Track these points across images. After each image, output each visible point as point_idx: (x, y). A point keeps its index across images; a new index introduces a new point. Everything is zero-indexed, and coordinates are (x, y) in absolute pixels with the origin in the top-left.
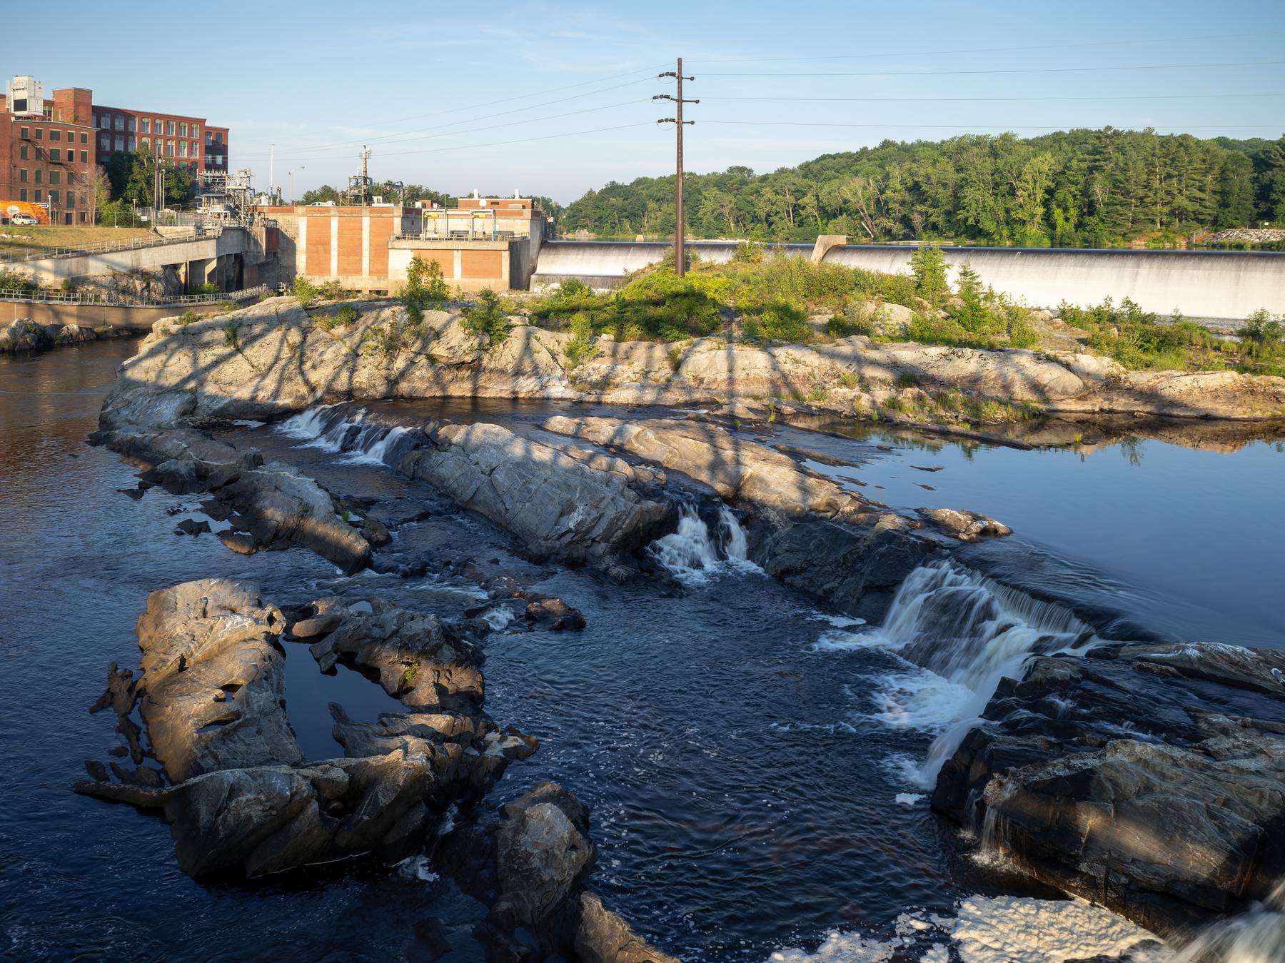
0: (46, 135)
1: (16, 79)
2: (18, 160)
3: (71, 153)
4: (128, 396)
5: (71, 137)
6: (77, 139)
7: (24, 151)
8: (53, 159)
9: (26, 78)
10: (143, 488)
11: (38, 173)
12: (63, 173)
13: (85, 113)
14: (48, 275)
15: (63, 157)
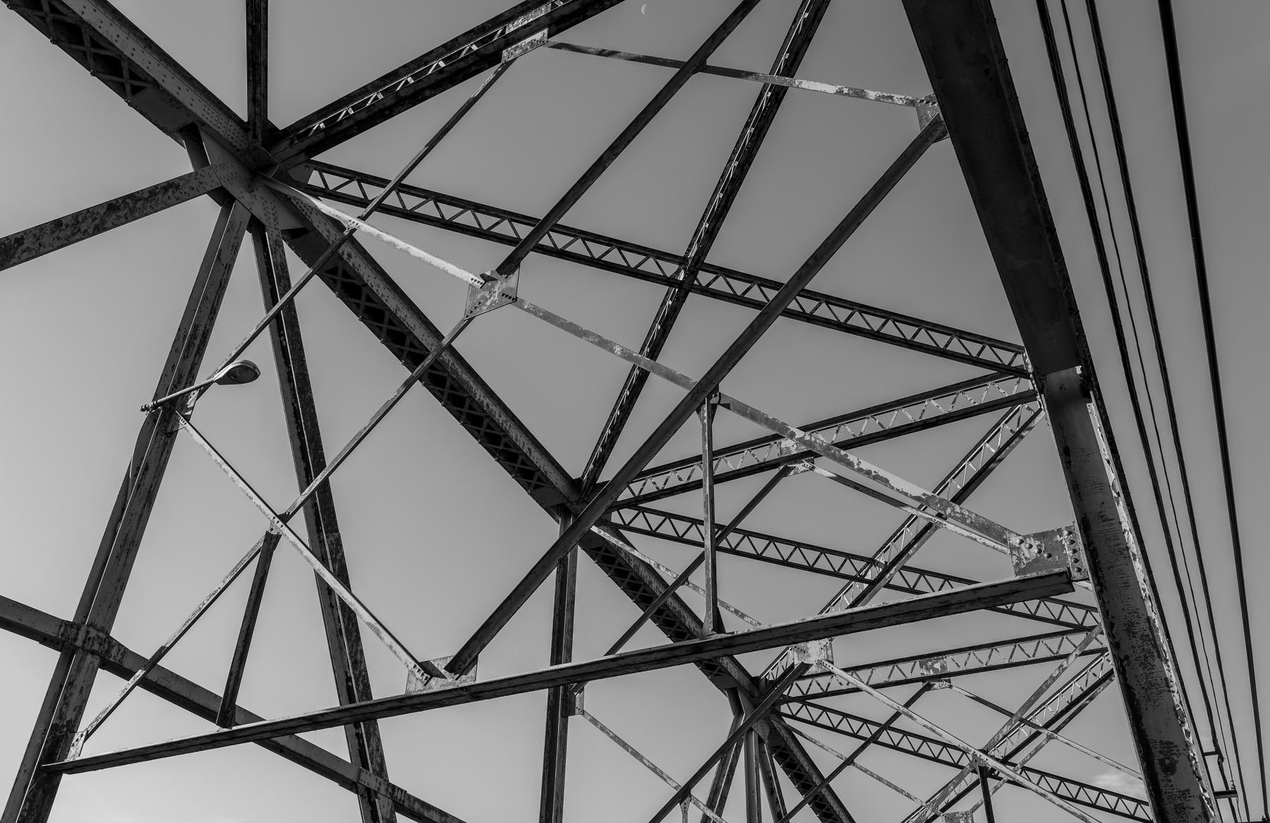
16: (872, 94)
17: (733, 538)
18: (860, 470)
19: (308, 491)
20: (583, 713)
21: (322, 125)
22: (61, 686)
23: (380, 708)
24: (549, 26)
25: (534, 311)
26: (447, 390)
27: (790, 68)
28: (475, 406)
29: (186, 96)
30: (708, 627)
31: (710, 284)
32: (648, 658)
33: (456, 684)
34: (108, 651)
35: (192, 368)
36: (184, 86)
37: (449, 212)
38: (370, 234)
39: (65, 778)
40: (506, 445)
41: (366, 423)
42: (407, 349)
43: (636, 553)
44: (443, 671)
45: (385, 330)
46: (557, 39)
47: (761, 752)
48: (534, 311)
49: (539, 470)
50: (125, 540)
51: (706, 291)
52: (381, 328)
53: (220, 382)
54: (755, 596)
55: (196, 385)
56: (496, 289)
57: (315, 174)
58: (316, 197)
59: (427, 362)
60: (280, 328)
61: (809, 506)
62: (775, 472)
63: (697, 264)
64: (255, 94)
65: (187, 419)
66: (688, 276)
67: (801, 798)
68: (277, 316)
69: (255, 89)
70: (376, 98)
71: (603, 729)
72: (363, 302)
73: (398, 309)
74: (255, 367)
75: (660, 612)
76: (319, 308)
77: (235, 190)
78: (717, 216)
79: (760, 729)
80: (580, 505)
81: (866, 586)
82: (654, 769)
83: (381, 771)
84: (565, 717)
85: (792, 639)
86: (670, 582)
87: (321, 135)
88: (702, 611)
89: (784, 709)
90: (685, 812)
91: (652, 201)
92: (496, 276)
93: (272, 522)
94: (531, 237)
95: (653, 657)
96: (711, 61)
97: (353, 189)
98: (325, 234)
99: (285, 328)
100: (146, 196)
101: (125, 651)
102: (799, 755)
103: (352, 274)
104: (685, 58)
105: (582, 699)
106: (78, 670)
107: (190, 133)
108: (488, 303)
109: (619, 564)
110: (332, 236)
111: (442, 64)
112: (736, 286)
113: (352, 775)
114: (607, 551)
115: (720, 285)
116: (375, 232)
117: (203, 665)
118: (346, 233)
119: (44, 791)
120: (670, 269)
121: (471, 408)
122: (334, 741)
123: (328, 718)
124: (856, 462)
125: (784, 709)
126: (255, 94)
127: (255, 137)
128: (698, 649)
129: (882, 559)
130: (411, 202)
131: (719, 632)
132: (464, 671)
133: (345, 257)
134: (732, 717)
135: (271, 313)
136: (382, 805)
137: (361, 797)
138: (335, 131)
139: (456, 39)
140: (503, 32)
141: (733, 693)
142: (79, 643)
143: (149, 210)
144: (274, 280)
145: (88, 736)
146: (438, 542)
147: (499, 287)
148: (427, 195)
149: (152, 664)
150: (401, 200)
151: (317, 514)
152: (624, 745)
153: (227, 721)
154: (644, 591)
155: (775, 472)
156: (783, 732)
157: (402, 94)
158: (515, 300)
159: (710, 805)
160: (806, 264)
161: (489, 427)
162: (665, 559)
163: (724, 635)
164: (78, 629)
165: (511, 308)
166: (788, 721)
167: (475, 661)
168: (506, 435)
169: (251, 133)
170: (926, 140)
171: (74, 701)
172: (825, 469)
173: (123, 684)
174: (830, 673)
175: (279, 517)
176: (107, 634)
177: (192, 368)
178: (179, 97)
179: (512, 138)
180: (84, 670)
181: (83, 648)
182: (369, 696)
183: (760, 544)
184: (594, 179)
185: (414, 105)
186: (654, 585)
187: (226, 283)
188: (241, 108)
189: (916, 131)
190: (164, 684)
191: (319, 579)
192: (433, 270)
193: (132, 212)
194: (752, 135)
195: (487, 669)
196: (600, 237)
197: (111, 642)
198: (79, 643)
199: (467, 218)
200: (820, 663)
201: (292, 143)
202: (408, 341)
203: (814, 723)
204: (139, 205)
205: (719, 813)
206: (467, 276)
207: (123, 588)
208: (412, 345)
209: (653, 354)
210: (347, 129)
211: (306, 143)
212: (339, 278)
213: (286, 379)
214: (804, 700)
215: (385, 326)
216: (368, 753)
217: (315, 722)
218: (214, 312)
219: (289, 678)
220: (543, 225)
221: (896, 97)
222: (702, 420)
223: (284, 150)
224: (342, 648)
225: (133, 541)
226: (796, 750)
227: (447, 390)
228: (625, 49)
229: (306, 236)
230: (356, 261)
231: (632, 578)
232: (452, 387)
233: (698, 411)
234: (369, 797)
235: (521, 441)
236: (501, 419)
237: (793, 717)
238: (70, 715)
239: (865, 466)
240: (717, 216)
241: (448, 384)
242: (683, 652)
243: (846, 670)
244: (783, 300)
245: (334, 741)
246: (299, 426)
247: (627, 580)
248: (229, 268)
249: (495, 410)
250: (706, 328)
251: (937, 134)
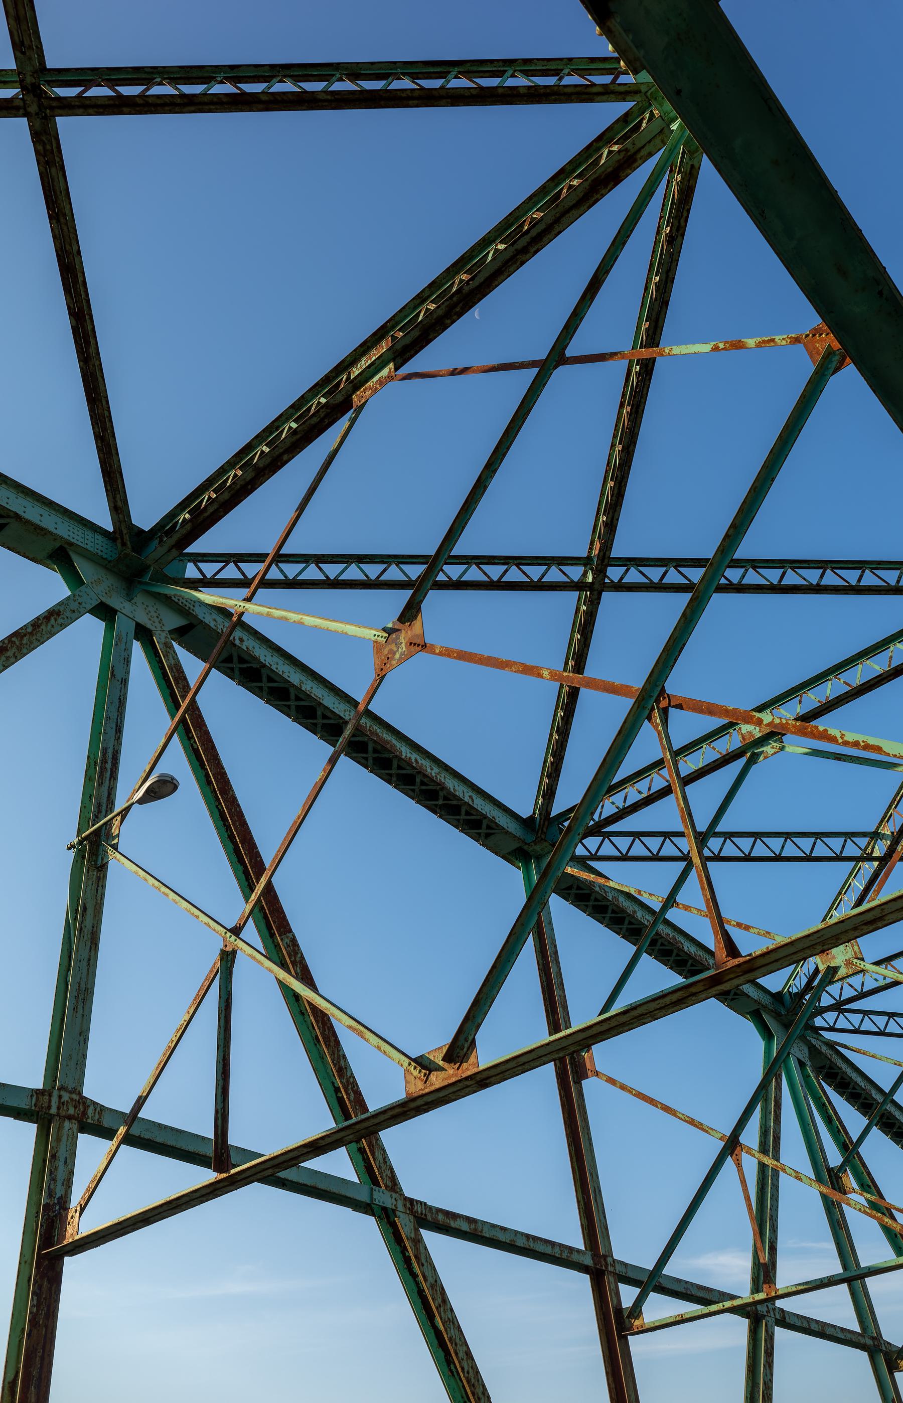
16: (751, 342)
17: (714, 844)
18: (846, 743)
19: (254, 897)
20: (597, 1074)
21: (187, 516)
22: (44, 1161)
23: (382, 1118)
24: (394, 359)
25: (448, 653)
26: (370, 755)
27: (653, 337)
28: (403, 764)
29: (49, 521)
30: (722, 954)
31: (622, 578)
32: (662, 1002)
33: (455, 1075)
34: (84, 1113)
35: (109, 794)
36: (45, 511)
37: (332, 570)
38: (259, 614)
39: (67, 1259)
40: (445, 798)
41: (298, 811)
42: (320, 721)
43: (612, 884)
44: (441, 1063)
45: (293, 708)
46: (405, 370)
47: (806, 1077)
48: (448, 653)
49: (485, 817)
50: (79, 989)
51: (620, 587)
52: (289, 707)
53: (141, 801)
54: (767, 907)
55: (117, 810)
56: (402, 640)
57: (190, 567)
58: (196, 589)
59: (347, 732)
60: (187, 731)
61: (789, 789)
62: (743, 761)
63: (603, 560)
64: (115, 502)
65: (115, 847)
66: (596, 576)
67: (865, 1121)
68: (183, 720)
69: (114, 498)
70: (235, 475)
71: (623, 1087)
72: (265, 684)
73: (301, 682)
74: (173, 778)
75: (653, 942)
76: (225, 703)
77: (115, 602)
78: (613, 506)
79: (799, 1051)
80: (540, 843)
81: (876, 864)
82: (692, 1122)
83: (394, 1186)
84: (578, 1082)
85: (820, 948)
86: (657, 906)
87: (188, 527)
88: (710, 940)
89: (818, 1022)
90: (739, 1165)
91: (544, 506)
92: (399, 626)
93: (225, 938)
94: (426, 576)
95: (667, 1000)
96: (569, 352)
97: (231, 572)
98: (212, 624)
99: (193, 731)
100: (30, 630)
101: (101, 1109)
102: (849, 1071)
103: (246, 657)
104: (542, 355)
106: (58, 1140)
107: (60, 557)
108: (397, 656)
109: (596, 900)
110: (222, 625)
111: (294, 425)
112: (656, 574)
113: (364, 1197)
114: (579, 888)
115: (634, 576)
116: (265, 610)
117: (184, 1106)
118: (235, 619)
119: (49, 1281)
120: (575, 573)
121: (400, 767)
122: (339, 1165)
123: (329, 1140)
124: (838, 735)
125: (818, 1022)
126: (115, 502)
127: (124, 544)
128: (716, 980)
129: (887, 831)
130: (291, 570)
131: (734, 958)
132: (464, 1058)
133: (237, 642)
134: (761, 1044)
135: (177, 719)
136: (404, 1223)
137: (379, 1218)
138: (201, 518)
139: (303, 396)
140: (348, 378)
141: (756, 1016)
142: (53, 1111)
143: (36, 643)
144: (173, 685)
145: (82, 1210)
146: (405, 927)
147: (403, 638)
148: (305, 559)
149: (132, 1117)
150: (282, 571)
151: (265, 917)
152: (652, 1101)
153: (225, 1165)
154: (630, 923)
155: (743, 761)
156: (824, 1049)
157: (261, 465)
158: (424, 646)
159: (764, 1149)
160: (727, 536)
161: (423, 783)
162: (645, 883)
163: (741, 960)
164: (50, 1095)
165: (422, 656)
166: (828, 1035)
167: (473, 1044)
168: (443, 788)
169: (119, 541)
170: (824, 375)
171: (61, 1175)
172: (796, 746)
173: (108, 1145)
174: (862, 971)
175: (230, 930)
176: (80, 1094)
177: (109, 794)
178: (42, 524)
179: (387, 480)
180: (64, 1139)
181: (58, 1115)
182: (365, 1109)
183: (745, 844)
184: (477, 502)
185: (274, 472)
186: (640, 914)
187: (125, 698)
188: (106, 522)
189: (809, 368)
190: (147, 1136)
191: (282, 985)
192: (330, 634)
193: (19, 649)
194: (630, 414)
195: (487, 1054)
196: (494, 557)
197: (85, 1103)
198: (53, 1111)
199: (353, 573)
200: (848, 963)
201: (161, 541)
202: (319, 713)
203: (857, 1031)
204: (25, 641)
205: (777, 1158)
206: (369, 634)
207: (86, 1041)
208: (324, 717)
209: (579, 668)
210: (212, 514)
211: (176, 537)
212: (236, 665)
213: (205, 782)
214: (839, 1007)
215: (293, 703)
216: (376, 1170)
217: (317, 1147)
218: (119, 730)
219: (280, 1108)
220: (433, 562)
221: (777, 338)
222: (656, 727)
223: (154, 550)
224: (322, 1057)
225: (87, 989)
226: (844, 1066)
227: (370, 755)
228: (476, 364)
229: (194, 631)
230: (249, 644)
231: (613, 912)
232: (375, 751)
233: (649, 718)
234: (388, 1217)
235: (460, 790)
236: (433, 771)
238: (59, 1191)
239: (850, 737)
240: (613, 506)
241: (370, 748)
242: (699, 987)
243: (878, 963)
244: (712, 576)
245: (339, 1165)
246: (228, 828)
247: (609, 915)
248: (125, 682)
249: (426, 764)
250: (631, 630)
251: (833, 365)
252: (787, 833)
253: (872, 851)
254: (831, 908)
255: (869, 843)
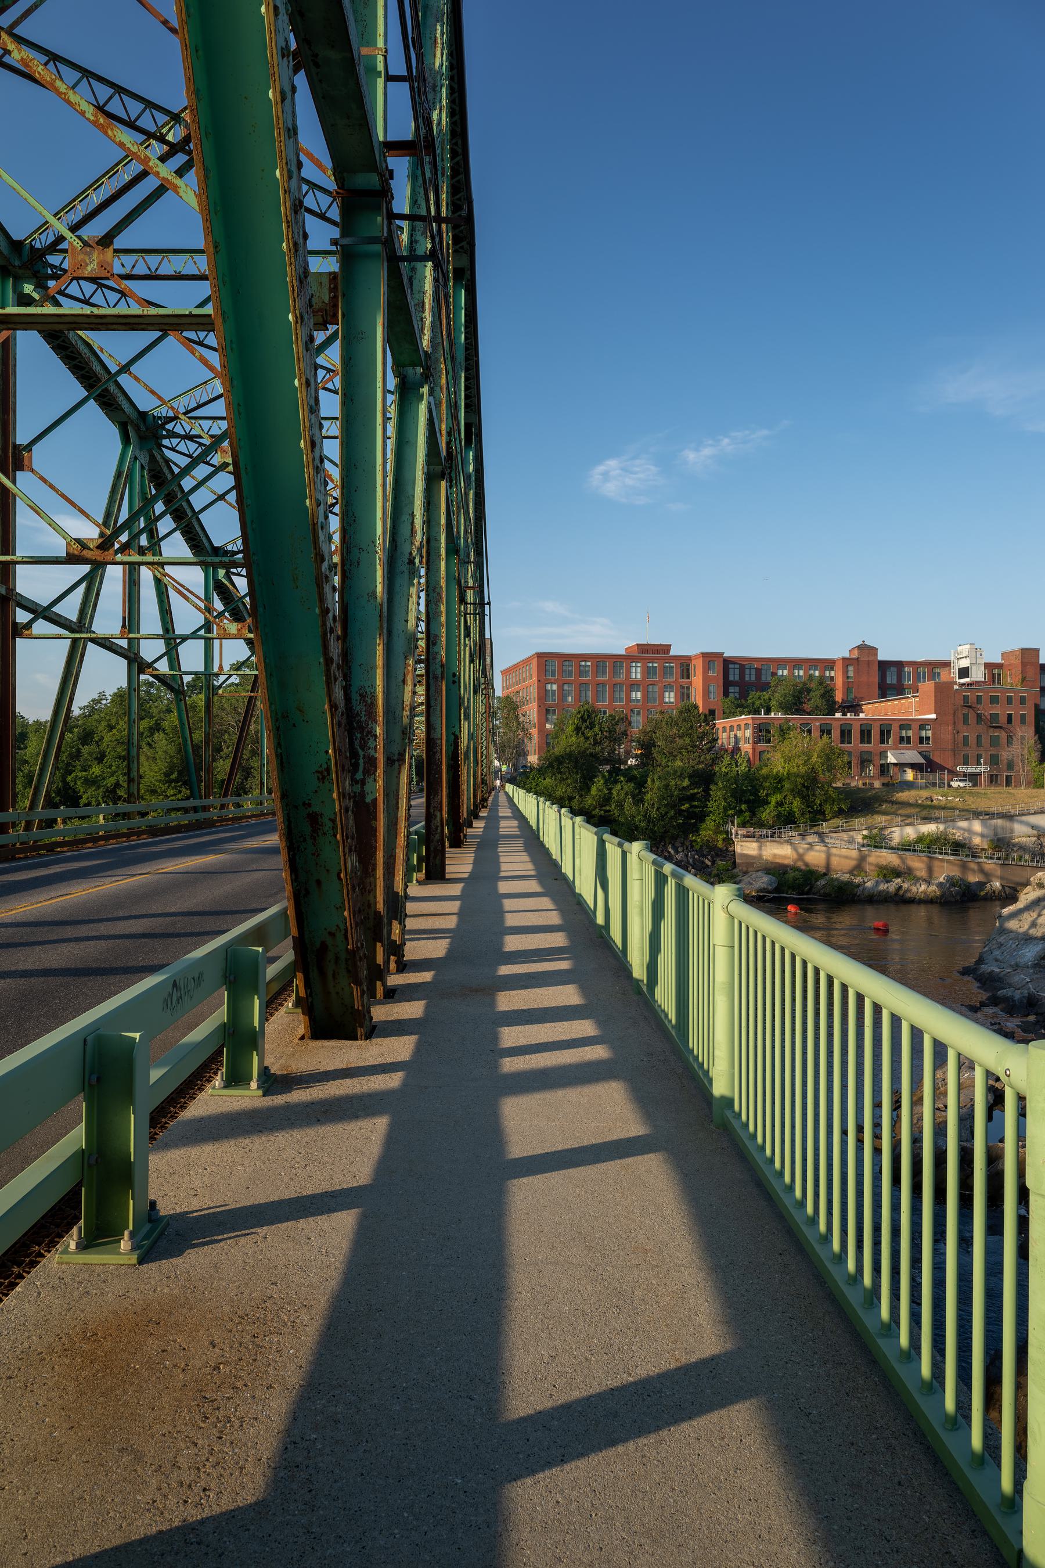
0: (986, 700)
1: (960, 648)
2: (960, 726)
3: (1010, 716)
4: (1001, 939)
5: (1009, 700)
6: (1003, 701)
7: (965, 717)
8: (994, 723)
9: (968, 646)
10: (983, 1004)
11: (979, 737)
12: (1003, 735)
13: (1032, 673)
14: (975, 831)
15: (1003, 720)
20: (32, 471)
47: (143, 476)
86: (113, 369)
92: (95, 245)
105: (30, 458)
125: (166, 442)
134: (119, 447)
154: (63, 341)
237: (173, 449)
252: (86, 71)
253: (167, 134)
254: (104, 176)
255: (167, 123)
